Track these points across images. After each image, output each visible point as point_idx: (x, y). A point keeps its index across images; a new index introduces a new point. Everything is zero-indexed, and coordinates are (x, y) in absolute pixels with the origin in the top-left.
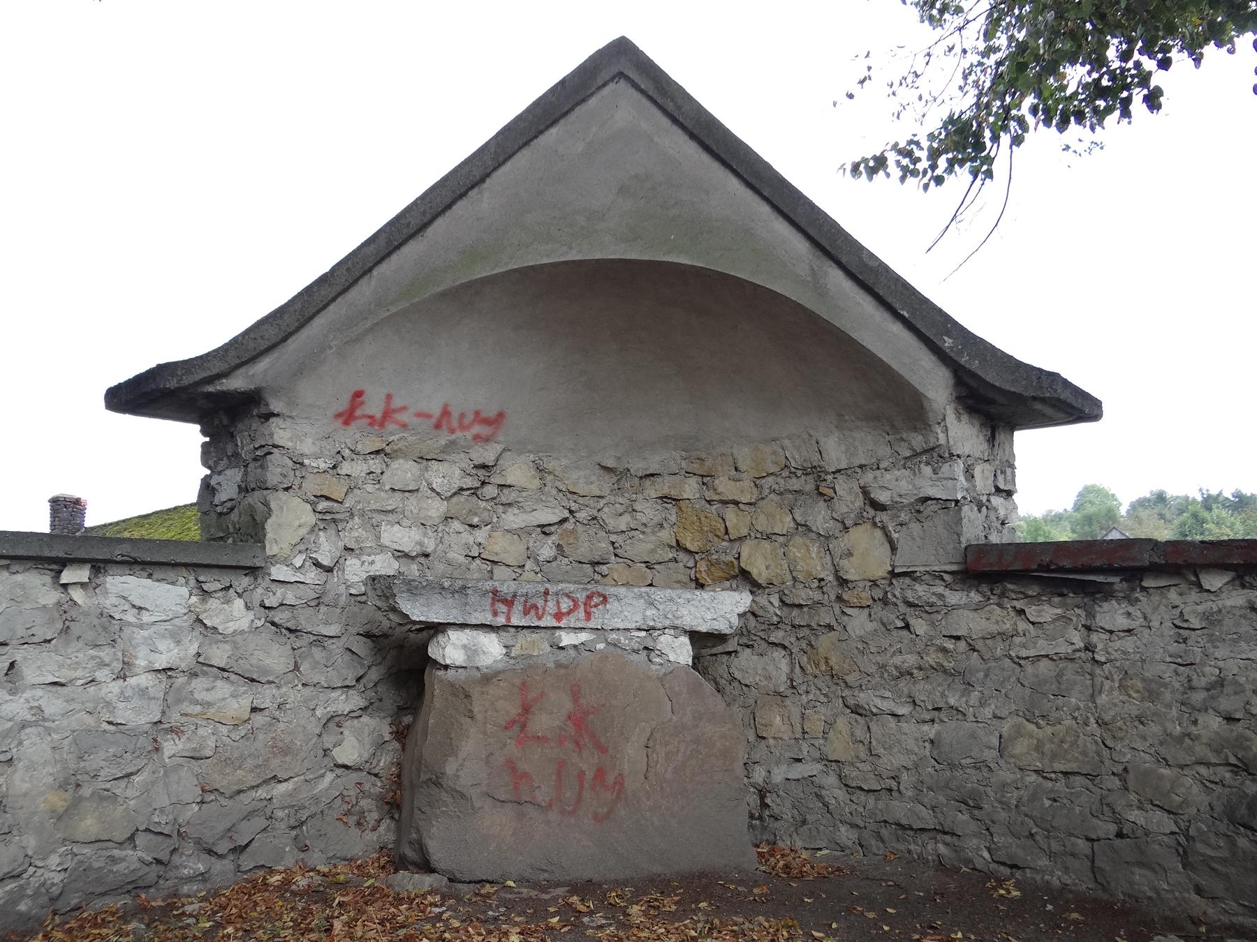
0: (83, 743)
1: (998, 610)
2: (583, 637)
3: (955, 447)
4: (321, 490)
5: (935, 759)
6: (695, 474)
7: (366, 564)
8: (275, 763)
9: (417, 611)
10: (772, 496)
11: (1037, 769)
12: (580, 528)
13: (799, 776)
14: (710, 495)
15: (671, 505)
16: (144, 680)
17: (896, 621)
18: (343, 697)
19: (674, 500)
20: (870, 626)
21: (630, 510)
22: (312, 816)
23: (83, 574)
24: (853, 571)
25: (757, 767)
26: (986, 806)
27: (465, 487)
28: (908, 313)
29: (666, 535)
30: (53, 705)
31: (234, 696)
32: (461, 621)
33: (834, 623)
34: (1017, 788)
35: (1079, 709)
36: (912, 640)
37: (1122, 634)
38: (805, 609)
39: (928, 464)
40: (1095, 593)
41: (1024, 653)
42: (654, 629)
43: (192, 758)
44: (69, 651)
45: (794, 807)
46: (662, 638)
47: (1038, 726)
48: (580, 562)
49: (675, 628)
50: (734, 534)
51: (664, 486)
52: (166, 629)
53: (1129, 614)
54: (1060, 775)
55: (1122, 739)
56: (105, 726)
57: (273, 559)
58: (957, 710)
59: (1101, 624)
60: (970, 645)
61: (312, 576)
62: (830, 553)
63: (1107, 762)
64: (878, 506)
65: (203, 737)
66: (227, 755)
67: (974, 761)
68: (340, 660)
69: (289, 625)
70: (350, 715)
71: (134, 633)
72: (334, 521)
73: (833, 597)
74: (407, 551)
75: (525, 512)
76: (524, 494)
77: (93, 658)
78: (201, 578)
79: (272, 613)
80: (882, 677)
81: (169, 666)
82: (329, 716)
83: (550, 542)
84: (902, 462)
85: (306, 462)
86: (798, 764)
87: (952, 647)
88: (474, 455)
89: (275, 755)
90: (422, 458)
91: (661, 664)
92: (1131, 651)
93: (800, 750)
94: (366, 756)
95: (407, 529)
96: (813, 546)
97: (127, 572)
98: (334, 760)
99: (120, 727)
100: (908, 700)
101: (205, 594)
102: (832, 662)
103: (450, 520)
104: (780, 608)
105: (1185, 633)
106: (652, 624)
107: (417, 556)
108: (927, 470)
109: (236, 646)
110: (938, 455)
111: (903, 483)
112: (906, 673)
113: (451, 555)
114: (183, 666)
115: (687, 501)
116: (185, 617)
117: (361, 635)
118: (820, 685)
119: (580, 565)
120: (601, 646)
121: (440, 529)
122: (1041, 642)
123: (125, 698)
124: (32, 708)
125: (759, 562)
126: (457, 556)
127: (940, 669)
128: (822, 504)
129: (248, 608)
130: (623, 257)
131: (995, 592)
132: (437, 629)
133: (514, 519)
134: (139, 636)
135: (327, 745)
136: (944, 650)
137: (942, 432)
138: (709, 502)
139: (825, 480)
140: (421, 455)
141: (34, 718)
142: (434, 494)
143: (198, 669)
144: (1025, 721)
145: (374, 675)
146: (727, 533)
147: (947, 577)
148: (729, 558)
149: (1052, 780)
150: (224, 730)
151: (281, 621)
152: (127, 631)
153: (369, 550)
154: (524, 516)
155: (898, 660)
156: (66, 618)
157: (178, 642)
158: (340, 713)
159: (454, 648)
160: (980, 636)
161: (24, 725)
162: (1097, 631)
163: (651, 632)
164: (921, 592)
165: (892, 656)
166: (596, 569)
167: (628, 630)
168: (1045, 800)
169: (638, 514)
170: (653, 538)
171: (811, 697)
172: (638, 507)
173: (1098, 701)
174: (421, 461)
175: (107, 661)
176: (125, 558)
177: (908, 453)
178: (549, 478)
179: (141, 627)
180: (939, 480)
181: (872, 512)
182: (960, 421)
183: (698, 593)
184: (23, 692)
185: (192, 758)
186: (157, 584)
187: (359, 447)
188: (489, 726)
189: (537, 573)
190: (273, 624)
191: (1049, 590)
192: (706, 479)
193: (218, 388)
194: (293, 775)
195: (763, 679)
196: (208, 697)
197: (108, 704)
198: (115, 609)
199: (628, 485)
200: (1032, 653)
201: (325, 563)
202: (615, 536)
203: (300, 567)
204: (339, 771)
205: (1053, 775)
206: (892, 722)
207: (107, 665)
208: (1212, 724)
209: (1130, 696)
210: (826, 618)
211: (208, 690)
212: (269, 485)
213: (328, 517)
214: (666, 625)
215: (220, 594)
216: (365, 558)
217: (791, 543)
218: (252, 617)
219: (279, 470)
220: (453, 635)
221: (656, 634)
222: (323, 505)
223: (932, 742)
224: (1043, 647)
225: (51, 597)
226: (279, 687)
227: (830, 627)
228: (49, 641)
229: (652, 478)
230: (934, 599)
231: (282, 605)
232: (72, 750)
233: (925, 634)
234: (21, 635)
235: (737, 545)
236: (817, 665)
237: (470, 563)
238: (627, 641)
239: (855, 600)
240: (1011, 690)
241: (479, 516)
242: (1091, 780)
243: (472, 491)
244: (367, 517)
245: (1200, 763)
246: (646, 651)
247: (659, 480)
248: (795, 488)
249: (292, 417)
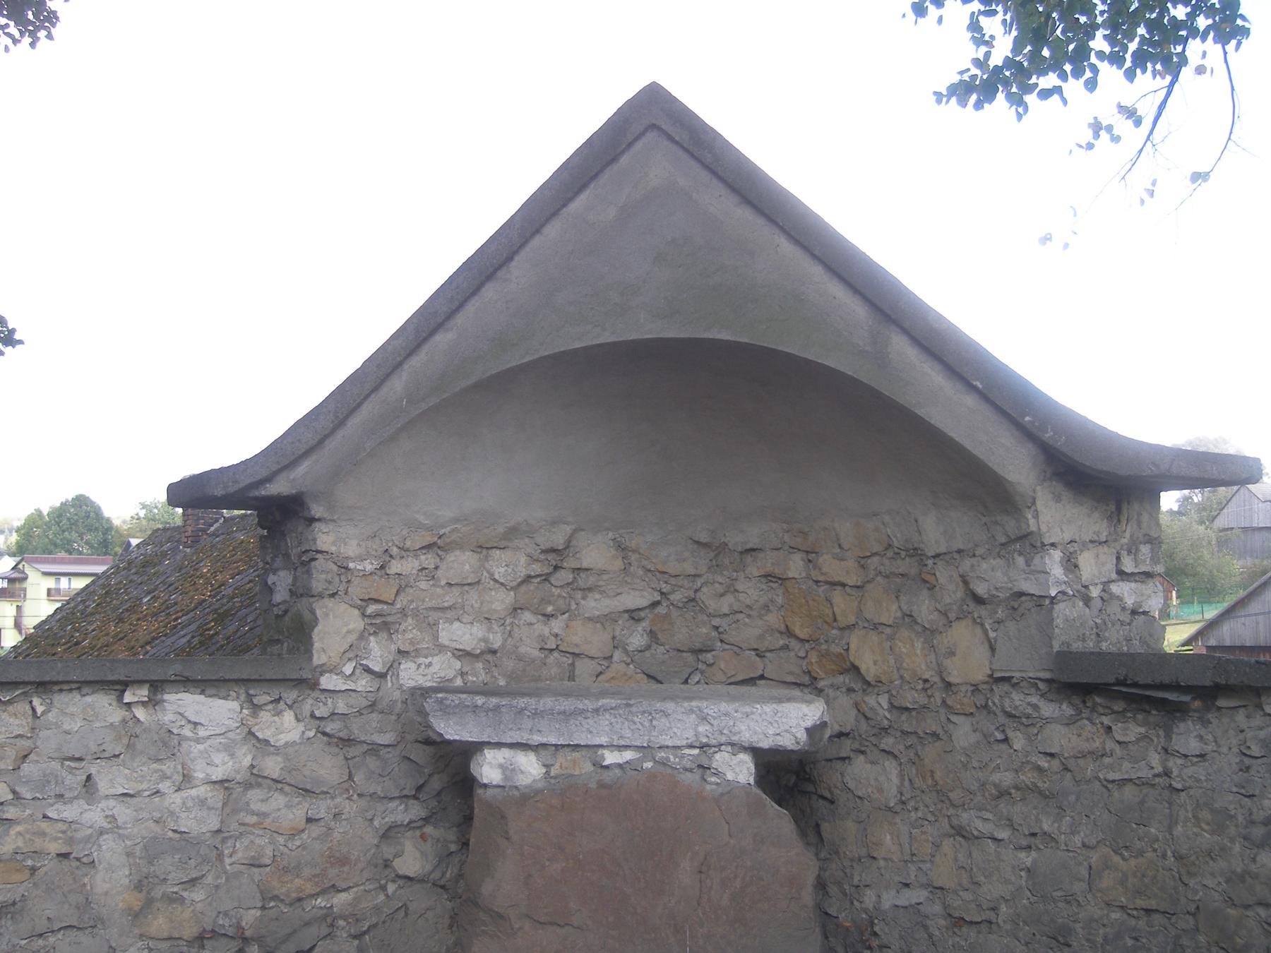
0: (152, 850)
1: (1089, 727)
2: (628, 755)
3: (1048, 534)
4: (369, 593)
5: (1030, 891)
6: (799, 550)
7: (423, 666)
8: (333, 872)
10: (879, 578)
11: (1121, 904)
12: (675, 613)
13: (907, 903)
14: (815, 575)
15: (777, 585)
16: (202, 791)
17: (996, 733)
18: (402, 807)
19: (780, 578)
20: (974, 738)
21: (732, 589)
22: (374, 926)
23: (143, 693)
24: (955, 672)
25: (868, 892)
26: (1075, 944)
27: (533, 574)
28: (981, 384)
29: (773, 619)
30: (123, 813)
31: (288, 806)
32: (496, 740)
33: (940, 731)
34: (1104, 925)
35: (1158, 840)
36: (1010, 756)
37: (1195, 760)
38: (914, 713)
39: (1020, 554)
40: (1175, 711)
41: (1111, 776)
42: (707, 745)
43: (251, 865)
44: (135, 765)
45: (901, 938)
46: (718, 756)
47: (1124, 859)
48: (679, 650)
49: (732, 745)
50: (842, 622)
51: (768, 562)
52: (220, 743)
53: (1201, 738)
54: (1142, 912)
55: (1195, 874)
56: (170, 834)
57: (323, 670)
58: (1050, 836)
59: (1176, 748)
60: (1064, 764)
61: (363, 683)
62: (935, 651)
63: (1183, 900)
64: (979, 600)
65: (260, 846)
66: (285, 863)
67: (1063, 894)
68: (397, 769)
69: (341, 735)
70: (409, 826)
71: (191, 746)
72: (385, 624)
73: (939, 702)
74: (469, 649)
75: (608, 597)
76: (605, 577)
77: (156, 771)
78: (251, 692)
79: (323, 724)
80: (984, 796)
81: (225, 778)
82: (387, 826)
83: (640, 629)
84: (997, 550)
85: (351, 565)
86: (906, 890)
87: (1046, 765)
88: (540, 540)
89: (332, 864)
90: (481, 547)
91: (717, 784)
92: (1203, 778)
93: (908, 874)
94: (429, 867)
95: (468, 626)
96: (918, 641)
97: (182, 690)
98: (395, 871)
99: (185, 835)
100: (1007, 823)
101: (256, 708)
102: (938, 775)
103: (519, 611)
104: (890, 712)
105: (1247, 761)
106: (705, 740)
107: (482, 653)
108: (1020, 561)
109: (287, 758)
110: (1030, 544)
111: (999, 574)
112: (1002, 794)
113: (522, 650)
114: (239, 778)
115: (794, 581)
116: (238, 731)
117: (420, 742)
118: (928, 801)
119: (680, 654)
120: (648, 765)
121: (507, 623)
122: (1126, 765)
123: (186, 808)
124: (107, 817)
126: (530, 649)
127: (1035, 789)
128: (925, 592)
129: (298, 720)
130: (661, 336)
131: (1088, 705)
132: (477, 747)
133: (594, 605)
134: (195, 751)
135: (387, 856)
136: (1040, 769)
137: (1034, 517)
138: (817, 582)
139: (926, 565)
140: (479, 544)
141: (110, 826)
142: (497, 586)
143: (253, 780)
144: (1112, 853)
145: (436, 784)
146: (835, 620)
147: (1041, 685)
148: (839, 650)
149: (1134, 917)
150: (281, 839)
151: (333, 732)
152: (185, 745)
153: (426, 652)
154: (607, 602)
155: (996, 777)
156: (130, 733)
157: (232, 755)
158: (399, 823)
159: (491, 767)
160: (1071, 754)
161: (102, 832)
162: (1173, 755)
163: (705, 749)
164: (1017, 700)
165: (991, 773)
166: (700, 657)
167: (679, 747)
168: (1128, 939)
169: (741, 595)
170: (760, 623)
171: (920, 814)
172: (740, 587)
173: (1175, 833)
174: (479, 550)
175: (169, 774)
176: (178, 678)
177: (1003, 540)
178: (634, 557)
179: (198, 741)
180: (1032, 572)
181: (972, 605)
182: (543, 717)
183: (758, 706)
184: (100, 802)
185: (251, 865)
186: (211, 699)
187: (408, 543)
188: (526, 847)
189: (628, 664)
190: (325, 734)
191: (1134, 706)
192: (811, 555)
193: (263, 493)
194: (351, 885)
195: (875, 791)
196: (263, 808)
197: (172, 813)
198: (173, 725)
199: (727, 561)
200: (1117, 776)
201: (377, 669)
202: (718, 620)
203: (350, 675)
204: (401, 882)
205: (1135, 913)
206: (992, 845)
207: (167, 778)
209: (1200, 827)
210: (931, 725)
211: (262, 801)
212: (314, 592)
213: (378, 621)
214: (722, 742)
215: (270, 707)
216: (421, 660)
217: (897, 636)
218: (303, 729)
219: (323, 576)
220: (489, 754)
221: (711, 751)
222: (372, 609)
223: (1029, 870)
224: (1126, 770)
225: (116, 715)
226: (333, 798)
227: (935, 735)
228: (118, 756)
229: (753, 554)
230: (1029, 710)
231: (333, 714)
232: (143, 854)
233: (1023, 749)
234: (95, 750)
235: (846, 633)
236: (924, 778)
237: (546, 657)
238: (677, 760)
239: (959, 707)
240: (1099, 816)
241: (553, 605)
242: (1169, 919)
243: (543, 578)
244: (422, 616)
245: (1260, 904)
246: (701, 770)
247: (761, 555)
248: (901, 571)
249: (334, 521)
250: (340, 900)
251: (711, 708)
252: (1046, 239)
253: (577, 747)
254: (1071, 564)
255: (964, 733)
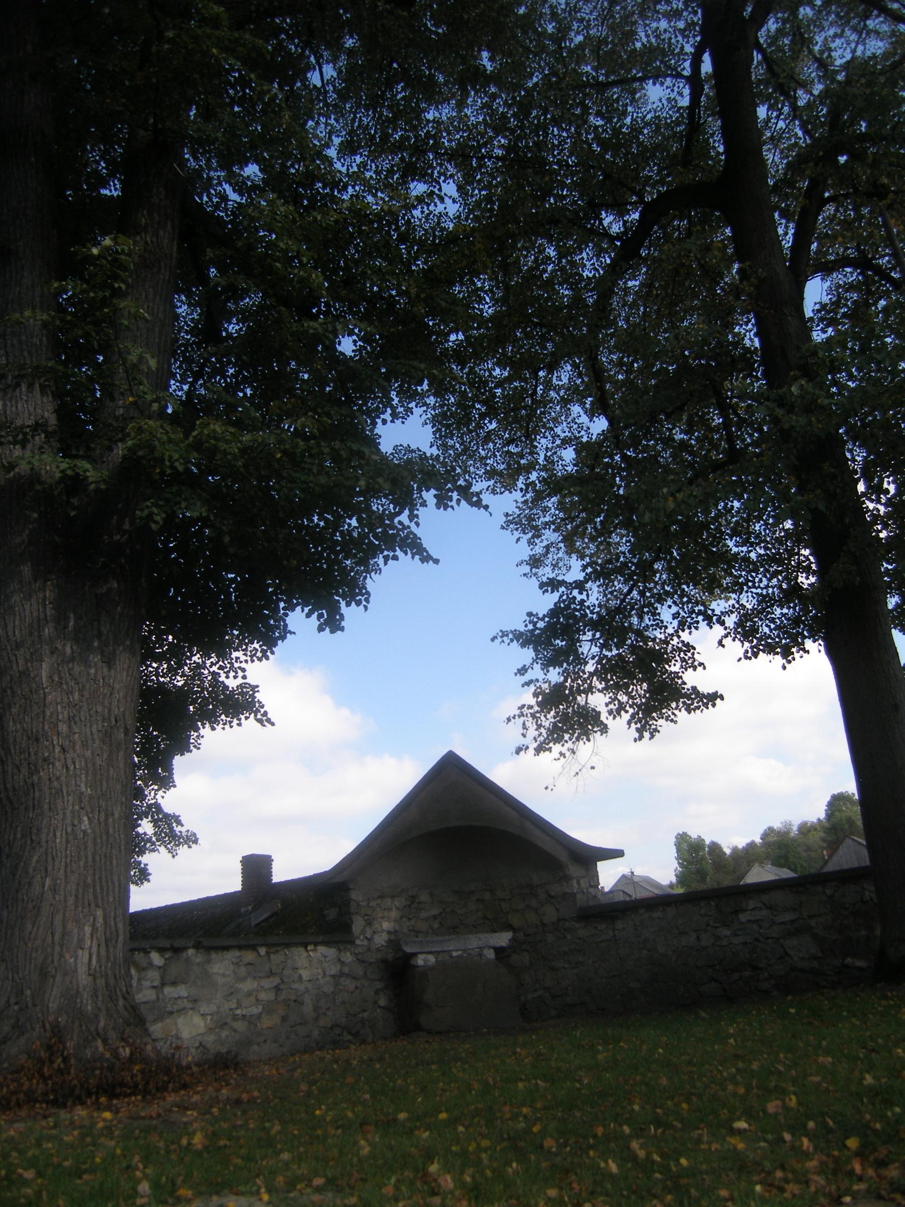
2: (460, 953)
9: (409, 949)
64: (552, 897)
101: (340, 950)
108: (565, 884)
125: (515, 921)
132: (414, 955)
133: (424, 914)
208: (645, 952)
220: (419, 956)
222: (366, 918)
250: (366, 1014)
251: (482, 936)
252: (546, 788)
253: (444, 952)
254: (578, 883)
255: (550, 938)
